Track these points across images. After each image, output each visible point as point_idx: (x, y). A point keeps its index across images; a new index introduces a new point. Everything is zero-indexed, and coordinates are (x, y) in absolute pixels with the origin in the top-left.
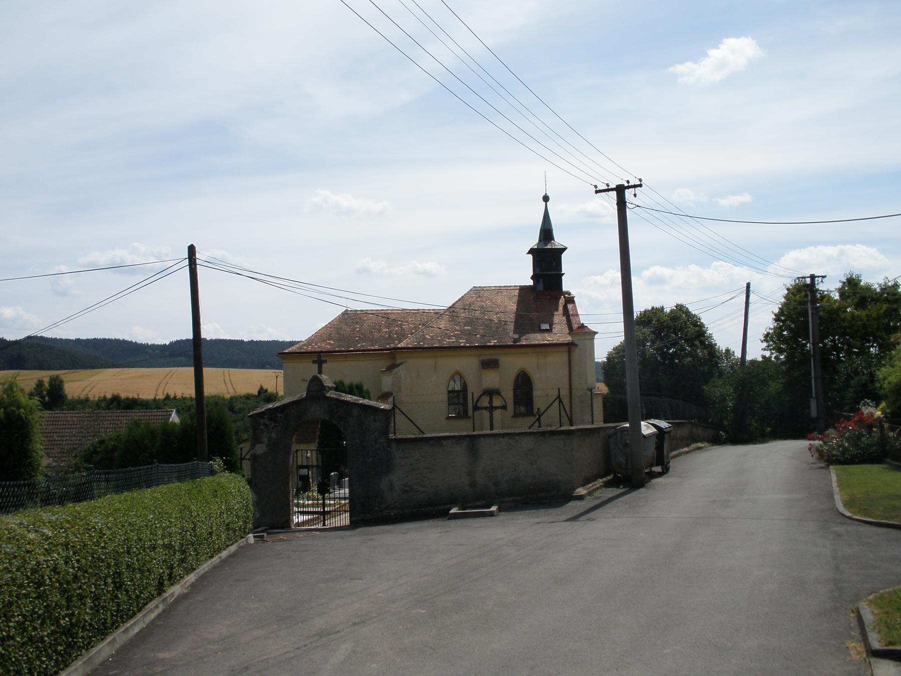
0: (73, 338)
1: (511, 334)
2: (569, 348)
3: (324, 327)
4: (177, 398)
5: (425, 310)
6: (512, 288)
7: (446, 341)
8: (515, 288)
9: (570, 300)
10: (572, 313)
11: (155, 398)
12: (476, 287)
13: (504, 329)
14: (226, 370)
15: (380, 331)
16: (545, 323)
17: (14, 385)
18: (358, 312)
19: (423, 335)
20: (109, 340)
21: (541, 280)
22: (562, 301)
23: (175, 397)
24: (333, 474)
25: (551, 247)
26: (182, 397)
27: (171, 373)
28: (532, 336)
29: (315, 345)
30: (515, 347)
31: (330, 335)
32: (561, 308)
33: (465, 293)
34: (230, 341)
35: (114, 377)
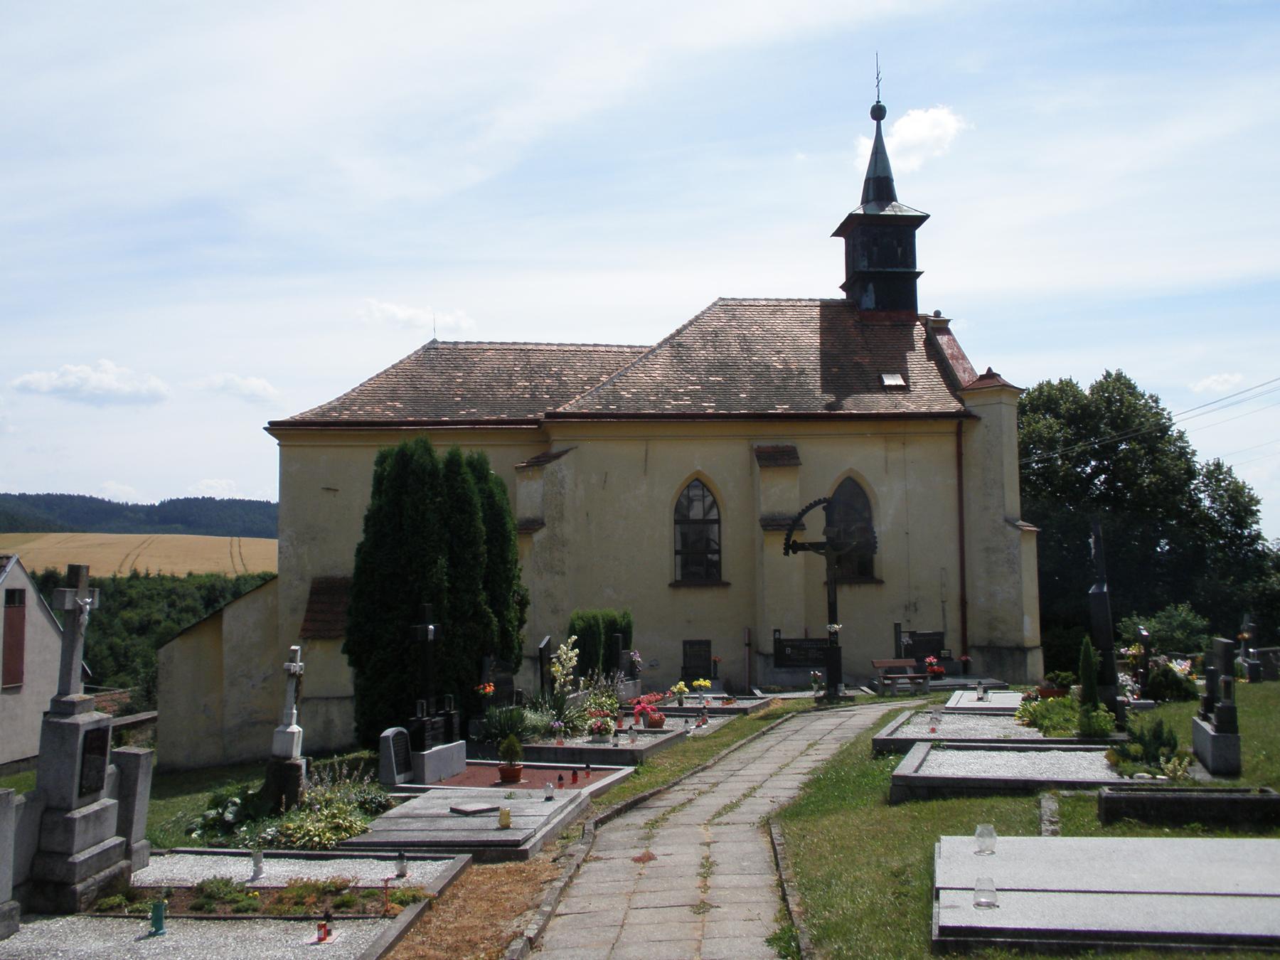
0: (16, 492)
1: (818, 393)
2: (960, 426)
3: (382, 373)
4: (151, 576)
5: (612, 346)
6: (804, 303)
7: (669, 404)
8: (811, 303)
9: (938, 326)
10: (950, 351)
11: (115, 576)
12: (723, 299)
13: (801, 385)
14: (236, 539)
15: (510, 385)
16: (892, 372)
17: (1111, 831)
18: (460, 347)
19: (615, 392)
20: (70, 497)
21: (871, 286)
22: (919, 331)
23: (148, 575)
24: (389, 732)
25: (893, 213)
26: (159, 575)
27: (149, 542)
28: (867, 398)
29: (360, 410)
30: (831, 418)
31: (394, 391)
32: (919, 345)
33: (703, 310)
34: (250, 503)
35: (59, 545)
